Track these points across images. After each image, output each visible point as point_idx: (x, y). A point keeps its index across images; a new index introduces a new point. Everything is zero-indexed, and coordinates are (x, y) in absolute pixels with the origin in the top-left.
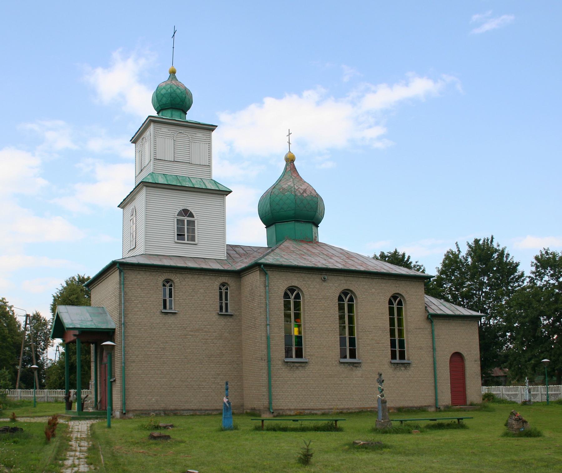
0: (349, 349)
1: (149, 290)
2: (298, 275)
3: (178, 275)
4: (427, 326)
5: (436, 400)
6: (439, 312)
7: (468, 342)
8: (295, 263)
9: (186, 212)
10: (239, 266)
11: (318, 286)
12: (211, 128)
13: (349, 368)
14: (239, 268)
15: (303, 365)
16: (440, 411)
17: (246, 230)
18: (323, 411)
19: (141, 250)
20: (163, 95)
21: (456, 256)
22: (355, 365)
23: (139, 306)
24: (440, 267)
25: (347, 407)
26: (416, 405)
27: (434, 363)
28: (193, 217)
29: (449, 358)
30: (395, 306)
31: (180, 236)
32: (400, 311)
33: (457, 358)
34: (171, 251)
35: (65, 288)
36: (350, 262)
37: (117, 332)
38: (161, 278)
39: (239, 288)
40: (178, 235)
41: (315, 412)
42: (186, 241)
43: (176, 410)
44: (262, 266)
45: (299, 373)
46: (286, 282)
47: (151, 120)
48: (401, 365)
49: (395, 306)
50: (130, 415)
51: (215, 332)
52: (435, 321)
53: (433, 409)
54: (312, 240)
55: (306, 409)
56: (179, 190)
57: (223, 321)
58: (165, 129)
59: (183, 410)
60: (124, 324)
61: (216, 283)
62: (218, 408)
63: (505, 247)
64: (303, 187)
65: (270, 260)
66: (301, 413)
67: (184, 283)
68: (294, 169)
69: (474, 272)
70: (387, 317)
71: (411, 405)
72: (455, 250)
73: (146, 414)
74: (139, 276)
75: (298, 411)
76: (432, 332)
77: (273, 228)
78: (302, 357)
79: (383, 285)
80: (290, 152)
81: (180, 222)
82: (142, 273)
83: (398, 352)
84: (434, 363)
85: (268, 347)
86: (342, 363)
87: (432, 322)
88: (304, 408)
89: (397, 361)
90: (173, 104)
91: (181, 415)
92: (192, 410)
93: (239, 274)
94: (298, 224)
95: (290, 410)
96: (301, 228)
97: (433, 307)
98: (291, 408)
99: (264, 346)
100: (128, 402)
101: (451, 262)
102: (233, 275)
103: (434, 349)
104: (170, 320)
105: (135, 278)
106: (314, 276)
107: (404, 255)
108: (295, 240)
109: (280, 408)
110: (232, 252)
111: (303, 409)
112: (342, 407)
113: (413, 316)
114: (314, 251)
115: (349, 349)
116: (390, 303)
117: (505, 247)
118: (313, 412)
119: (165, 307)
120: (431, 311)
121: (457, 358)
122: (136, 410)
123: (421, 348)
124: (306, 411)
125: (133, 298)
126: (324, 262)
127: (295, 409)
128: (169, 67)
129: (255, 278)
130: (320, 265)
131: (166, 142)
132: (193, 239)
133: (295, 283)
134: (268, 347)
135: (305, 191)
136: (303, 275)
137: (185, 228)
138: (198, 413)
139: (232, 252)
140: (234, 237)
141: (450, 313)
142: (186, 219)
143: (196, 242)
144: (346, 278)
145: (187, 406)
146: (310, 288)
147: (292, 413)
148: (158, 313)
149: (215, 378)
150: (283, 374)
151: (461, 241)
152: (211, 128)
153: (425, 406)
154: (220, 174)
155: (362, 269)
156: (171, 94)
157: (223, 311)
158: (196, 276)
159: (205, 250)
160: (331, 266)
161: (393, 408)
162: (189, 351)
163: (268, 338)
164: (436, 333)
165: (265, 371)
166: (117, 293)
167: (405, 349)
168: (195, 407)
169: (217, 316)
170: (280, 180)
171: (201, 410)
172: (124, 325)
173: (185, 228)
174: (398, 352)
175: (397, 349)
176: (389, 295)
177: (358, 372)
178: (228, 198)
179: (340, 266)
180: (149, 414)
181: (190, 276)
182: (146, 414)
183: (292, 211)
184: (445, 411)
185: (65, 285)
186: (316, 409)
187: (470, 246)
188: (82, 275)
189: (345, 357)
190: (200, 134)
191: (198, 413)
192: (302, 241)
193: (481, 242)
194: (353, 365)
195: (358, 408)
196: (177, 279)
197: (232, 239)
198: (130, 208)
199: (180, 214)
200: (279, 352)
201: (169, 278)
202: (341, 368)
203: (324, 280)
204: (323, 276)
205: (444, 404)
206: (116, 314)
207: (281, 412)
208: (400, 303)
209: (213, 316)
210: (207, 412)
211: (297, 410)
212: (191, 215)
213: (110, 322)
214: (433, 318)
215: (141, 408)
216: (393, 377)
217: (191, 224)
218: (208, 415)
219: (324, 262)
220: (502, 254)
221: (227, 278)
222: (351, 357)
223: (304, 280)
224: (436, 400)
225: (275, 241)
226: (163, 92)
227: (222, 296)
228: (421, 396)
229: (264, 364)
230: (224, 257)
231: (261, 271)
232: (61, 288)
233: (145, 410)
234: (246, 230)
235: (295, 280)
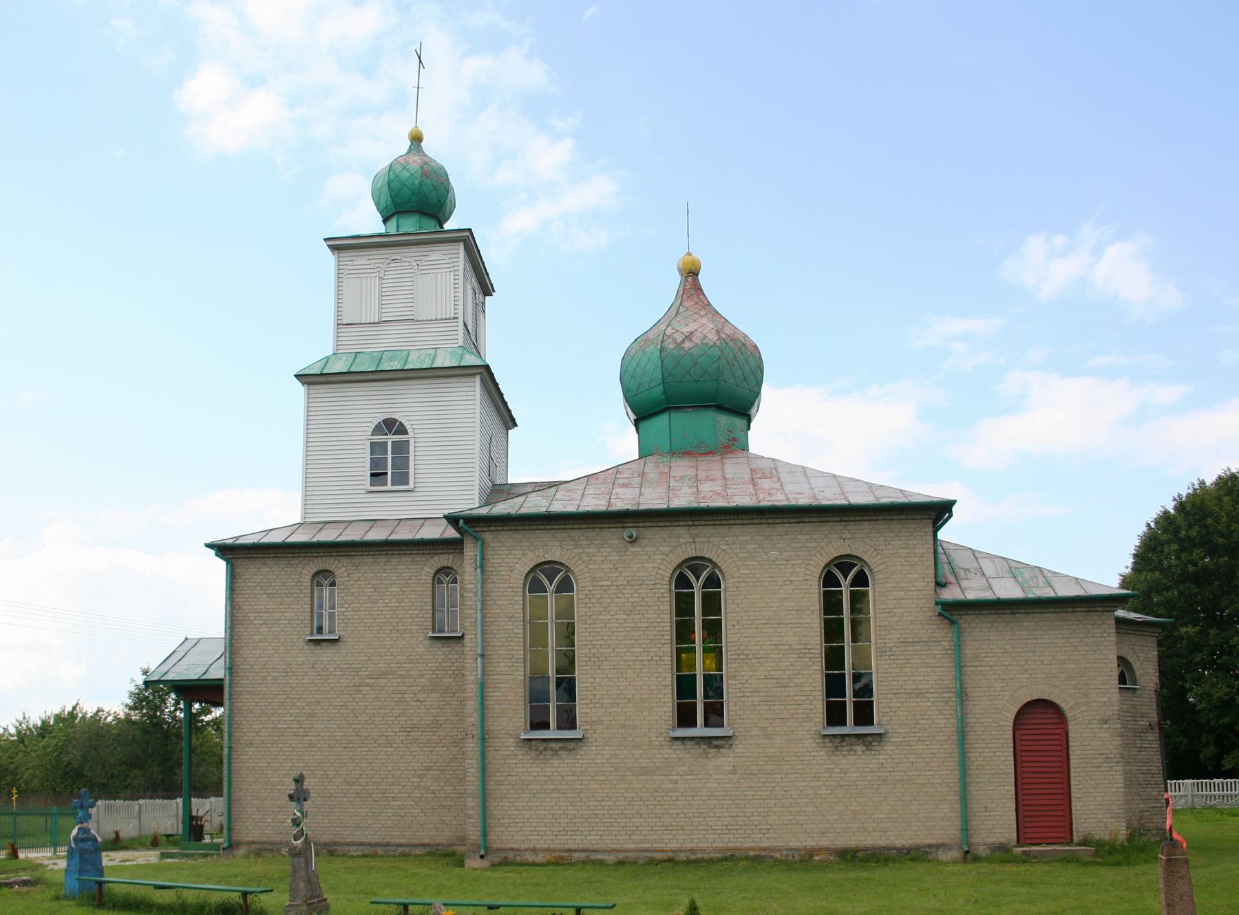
0: (698, 702)
2: (561, 535)
3: (345, 561)
4: (942, 634)
5: (966, 829)
9: (391, 425)
11: (614, 557)
13: (697, 750)
15: (572, 745)
16: (977, 859)
17: (576, 439)
18: (621, 856)
22: (715, 742)
23: (264, 629)
25: (689, 845)
26: (899, 843)
27: (963, 732)
28: (406, 433)
29: (1011, 717)
30: (845, 588)
31: (377, 476)
32: (858, 600)
33: (1040, 725)
40: (372, 475)
41: (600, 857)
42: (389, 487)
43: (336, 844)
44: (461, 522)
45: (560, 765)
46: (530, 555)
48: (854, 740)
49: (845, 588)
50: (242, 851)
51: (422, 676)
52: (967, 621)
53: (955, 854)
55: (576, 851)
59: (348, 844)
60: (482, 655)
62: (426, 841)
66: (562, 858)
67: (355, 576)
68: (698, 289)
71: (883, 842)
73: (272, 850)
74: (265, 570)
75: (557, 854)
76: (959, 646)
78: (574, 727)
79: (803, 537)
80: (689, 254)
82: (270, 562)
83: (848, 704)
84: (963, 732)
86: (677, 739)
87: (952, 622)
88: (572, 847)
89: (849, 728)
91: (344, 855)
92: (370, 844)
95: (534, 850)
98: (538, 846)
100: (237, 826)
103: (962, 695)
104: (326, 655)
106: (606, 533)
109: (509, 846)
111: (569, 850)
112: (674, 845)
115: (698, 702)
118: (594, 857)
121: (1040, 725)
122: (253, 842)
123: (918, 694)
124: (576, 855)
125: (252, 616)
127: (547, 850)
136: (575, 533)
138: (380, 851)
142: (390, 439)
143: (411, 485)
144: (694, 531)
145: (359, 836)
147: (540, 858)
148: (301, 644)
149: (419, 776)
153: (930, 846)
158: (382, 559)
161: (828, 850)
162: (363, 718)
164: (968, 651)
167: (874, 698)
168: (370, 838)
169: (427, 642)
171: (388, 845)
172: (231, 669)
174: (848, 704)
177: (723, 761)
180: (279, 850)
181: (370, 560)
182: (272, 850)
184: (989, 860)
186: (604, 851)
189: (545, 726)
191: (380, 851)
194: (709, 745)
195: (721, 850)
199: (378, 430)
200: (511, 714)
201: (325, 567)
202: (679, 751)
203: (633, 541)
204: (626, 534)
205: (991, 840)
207: (511, 855)
210: (400, 849)
211: (554, 850)
212: (402, 430)
215: (264, 839)
216: (829, 771)
217: (401, 449)
218: (405, 855)
219: (596, 502)
221: (451, 557)
222: (707, 725)
223: (576, 546)
224: (966, 829)
228: (924, 819)
233: (271, 843)
234: (576, 439)
235: (552, 547)
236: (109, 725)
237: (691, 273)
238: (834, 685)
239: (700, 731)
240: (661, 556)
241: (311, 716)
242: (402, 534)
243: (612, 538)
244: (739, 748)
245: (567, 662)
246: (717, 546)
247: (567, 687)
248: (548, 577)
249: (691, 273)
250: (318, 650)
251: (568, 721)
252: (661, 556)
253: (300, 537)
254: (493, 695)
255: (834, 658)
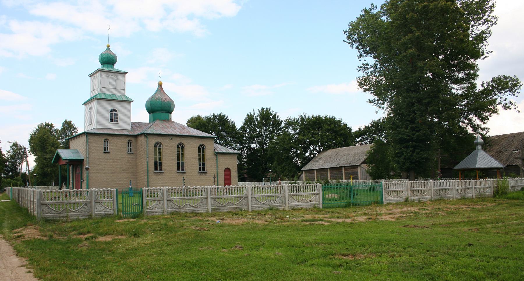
0: (180, 166)
1: (98, 144)
4: (215, 157)
6: (220, 152)
7: (233, 164)
8: (159, 133)
9: (114, 110)
10: (137, 133)
12: (125, 73)
14: (136, 134)
19: (94, 126)
20: (104, 58)
21: (252, 116)
24: (244, 121)
30: (201, 149)
31: (112, 121)
32: (203, 151)
33: (228, 171)
34: (107, 126)
35: (37, 130)
36: (183, 131)
37: (85, 161)
38: (103, 139)
39: (136, 142)
45: (160, 176)
47: (99, 70)
49: (201, 149)
52: (218, 155)
54: (169, 120)
56: (112, 101)
57: (129, 156)
58: (105, 74)
61: (127, 140)
63: (276, 113)
64: (165, 97)
65: (149, 131)
68: (162, 89)
69: (261, 125)
70: (197, 153)
72: (253, 114)
77: (151, 114)
81: (111, 114)
83: (202, 168)
85: (148, 167)
89: (202, 171)
90: (108, 61)
93: (136, 136)
94: (162, 113)
96: (163, 115)
97: (218, 149)
99: (146, 166)
101: (249, 120)
102: (133, 138)
104: (107, 155)
105: (92, 138)
107: (224, 116)
108: (161, 120)
110: (133, 126)
113: (209, 153)
114: (168, 126)
115: (180, 166)
116: (199, 148)
117: (276, 113)
119: (105, 150)
120: (216, 151)
121: (228, 171)
126: (172, 131)
128: (107, 44)
129: (142, 139)
130: (170, 133)
131: (107, 80)
132: (117, 121)
133: (159, 141)
134: (148, 167)
135: (166, 99)
137: (114, 117)
139: (133, 126)
140: (135, 119)
141: (225, 152)
142: (114, 113)
146: (165, 142)
150: (153, 176)
151: (254, 109)
152: (125, 73)
154: (129, 94)
155: (187, 134)
156: (107, 58)
157: (130, 153)
159: (123, 126)
160: (174, 134)
163: (147, 163)
164: (218, 160)
165: (146, 176)
166: (85, 145)
170: (155, 94)
172: (87, 158)
173: (114, 117)
174: (202, 168)
175: (202, 167)
176: (199, 145)
178: (132, 103)
179: (178, 133)
183: (160, 108)
185: (37, 128)
187: (259, 112)
188: (47, 122)
190: (120, 76)
192: (164, 121)
193: (265, 109)
196: (110, 138)
197: (133, 120)
198: (88, 106)
203: (171, 139)
206: (84, 153)
208: (203, 148)
209: (125, 154)
212: (116, 111)
213: (82, 156)
214: (217, 154)
217: (116, 115)
220: (275, 116)
225: (153, 120)
226: (104, 56)
227: (129, 145)
229: (146, 173)
230: (130, 128)
231: (145, 136)
232: (35, 130)
234: (140, 115)
235: (159, 140)
236: (37, 165)
237: (160, 85)
238: (178, 164)
239: (181, 171)
240: (176, 142)
241: (104, 167)
242: (116, 133)
243: (168, 138)
244: (187, 174)
245: (160, 159)
246: (184, 141)
247: (160, 163)
248: (181, 146)
249: (160, 85)
250: (105, 154)
251: (161, 169)
252: (176, 142)
253: (92, 132)
254: (149, 164)
255: (178, 159)
